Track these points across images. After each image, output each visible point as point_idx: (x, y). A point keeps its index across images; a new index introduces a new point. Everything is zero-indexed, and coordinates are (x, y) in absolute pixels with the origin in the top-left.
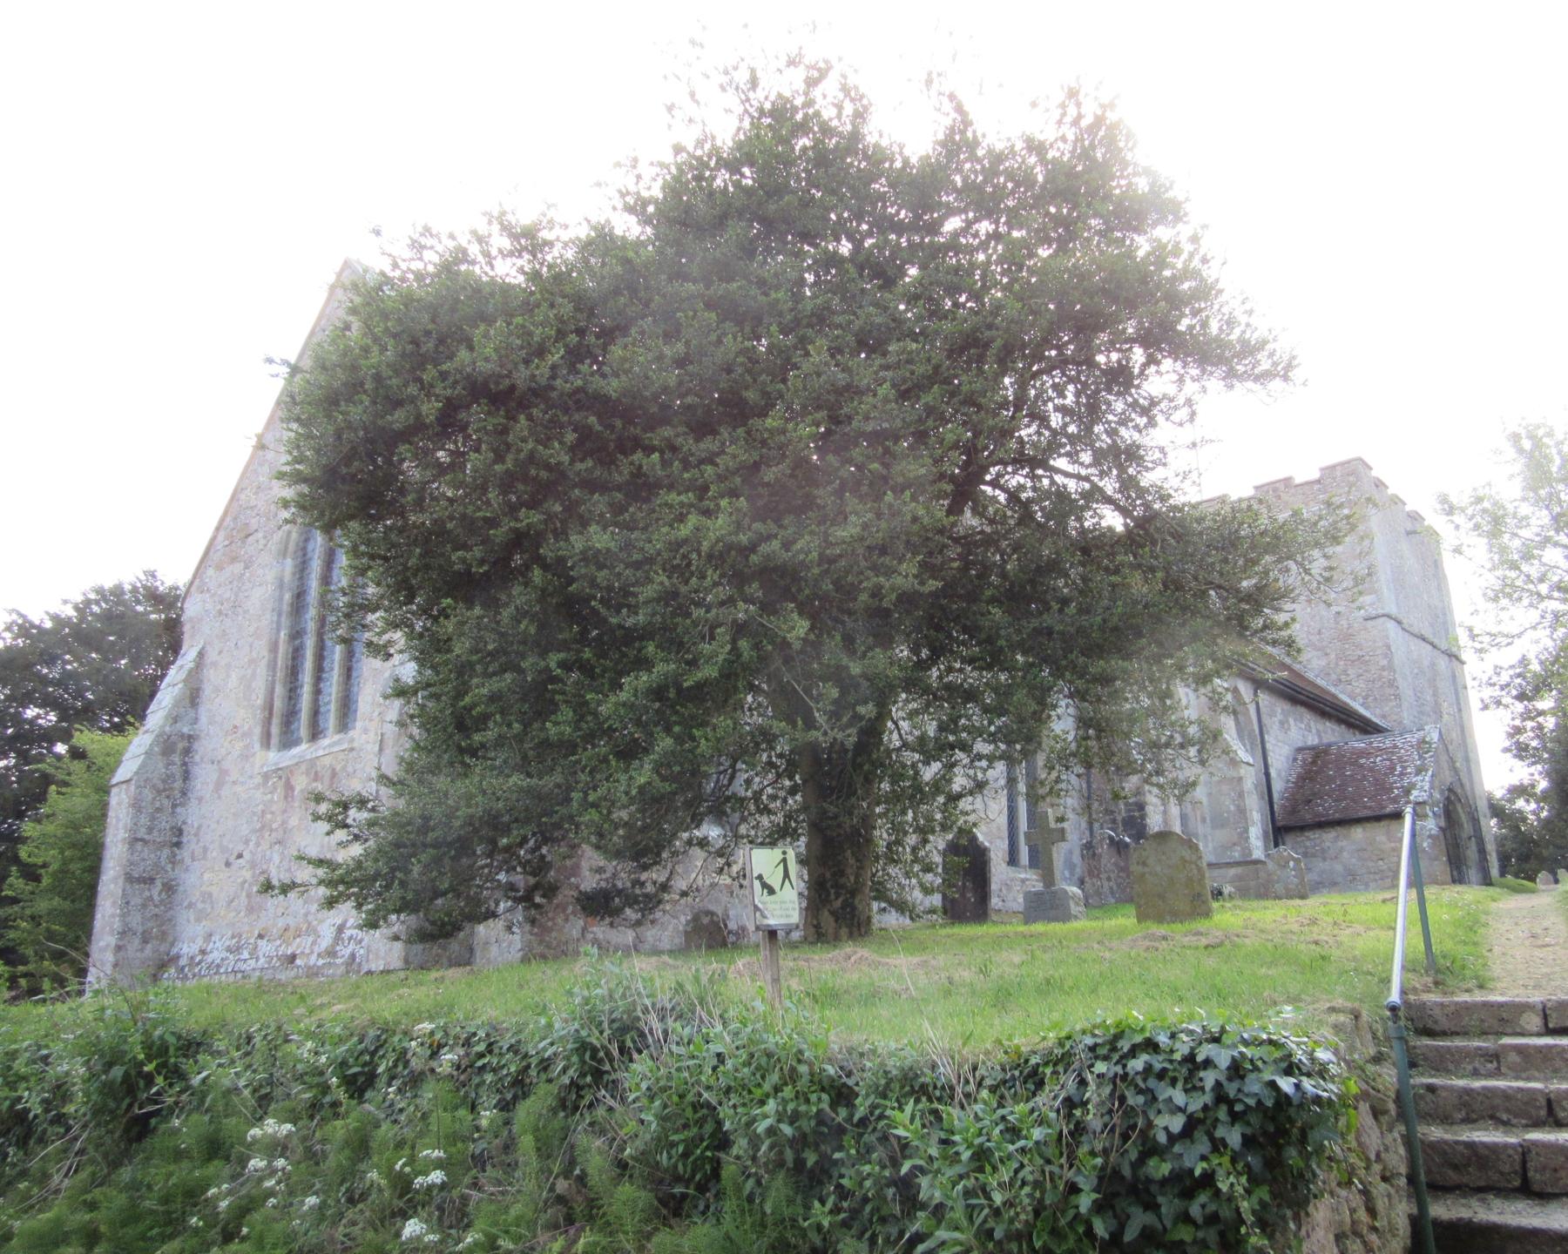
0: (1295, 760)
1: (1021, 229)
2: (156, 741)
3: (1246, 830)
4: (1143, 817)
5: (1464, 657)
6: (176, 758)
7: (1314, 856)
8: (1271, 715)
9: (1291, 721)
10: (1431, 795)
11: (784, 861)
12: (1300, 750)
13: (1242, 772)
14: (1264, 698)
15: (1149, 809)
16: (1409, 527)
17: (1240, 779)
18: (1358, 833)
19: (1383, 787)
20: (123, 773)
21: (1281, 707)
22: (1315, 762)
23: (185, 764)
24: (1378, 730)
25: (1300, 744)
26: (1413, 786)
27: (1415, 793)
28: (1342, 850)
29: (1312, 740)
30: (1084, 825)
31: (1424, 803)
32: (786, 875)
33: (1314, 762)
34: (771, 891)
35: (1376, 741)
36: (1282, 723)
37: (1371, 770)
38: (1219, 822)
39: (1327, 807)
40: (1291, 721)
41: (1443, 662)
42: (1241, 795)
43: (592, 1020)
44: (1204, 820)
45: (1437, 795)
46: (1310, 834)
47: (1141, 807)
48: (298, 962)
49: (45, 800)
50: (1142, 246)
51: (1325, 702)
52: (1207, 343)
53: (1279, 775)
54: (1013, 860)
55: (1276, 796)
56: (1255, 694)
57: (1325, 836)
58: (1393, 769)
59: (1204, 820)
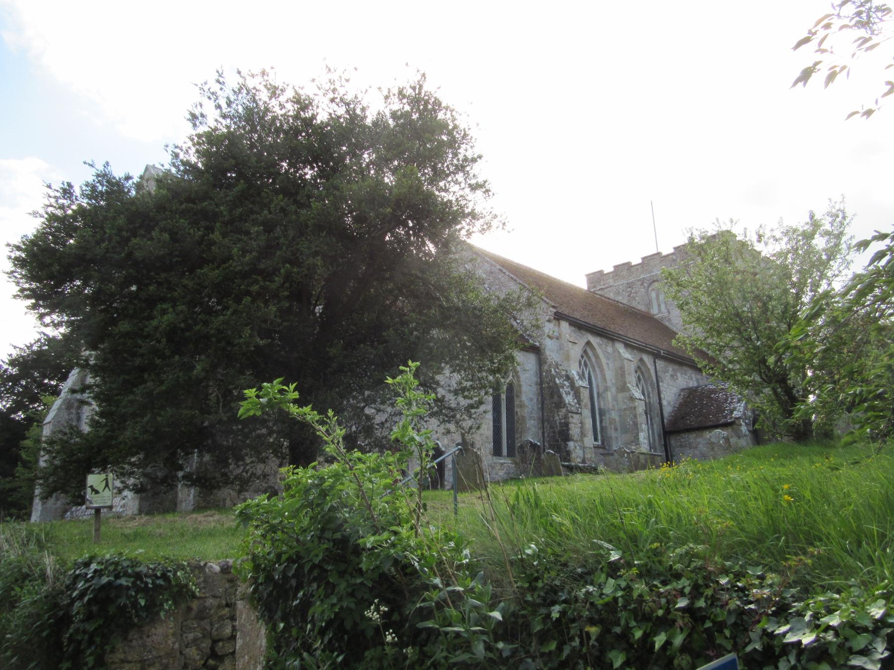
0: (680, 395)
1: (345, 159)
2: (63, 402)
3: (638, 435)
4: (568, 429)
6: (74, 411)
7: (685, 446)
8: (666, 371)
9: (679, 375)
10: (744, 414)
11: (107, 479)
12: (683, 390)
13: (636, 404)
14: (660, 364)
15: (571, 426)
17: (635, 408)
19: (721, 410)
20: (48, 419)
21: (671, 368)
23: (78, 413)
26: (735, 409)
27: (735, 412)
28: (699, 443)
30: (540, 434)
31: (740, 418)
32: (107, 485)
33: (688, 397)
34: (97, 492)
36: (672, 376)
37: (716, 400)
38: (625, 430)
39: (691, 421)
40: (679, 375)
42: (635, 416)
45: (749, 413)
46: (683, 435)
47: (567, 424)
48: (114, 510)
50: (34, 285)
52: (448, 213)
53: (669, 403)
54: (497, 452)
56: (655, 362)
57: (691, 436)
58: (726, 400)
59: (616, 429)
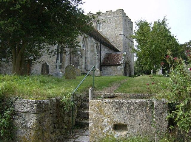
5: (134, 42)
12: (106, 54)
14: (102, 45)
16: (128, 21)
18: (112, 67)
19: (117, 60)
22: (108, 56)
24: (119, 52)
25: (107, 53)
29: (108, 52)
35: (117, 53)
36: (104, 49)
39: (108, 63)
41: (131, 42)
43: (90, 13)
44: (89, 63)
49: (84, 126)
51: (110, 46)
55: (101, 60)
59: (89, 63)
